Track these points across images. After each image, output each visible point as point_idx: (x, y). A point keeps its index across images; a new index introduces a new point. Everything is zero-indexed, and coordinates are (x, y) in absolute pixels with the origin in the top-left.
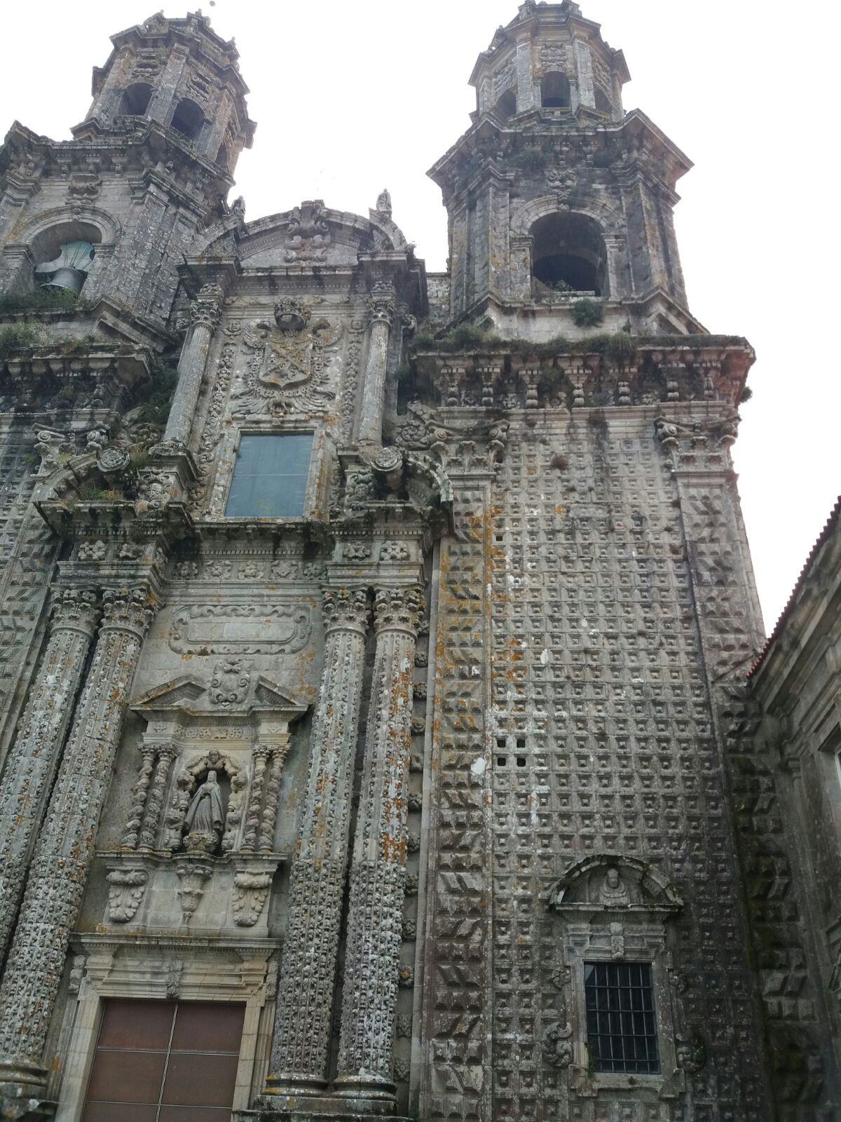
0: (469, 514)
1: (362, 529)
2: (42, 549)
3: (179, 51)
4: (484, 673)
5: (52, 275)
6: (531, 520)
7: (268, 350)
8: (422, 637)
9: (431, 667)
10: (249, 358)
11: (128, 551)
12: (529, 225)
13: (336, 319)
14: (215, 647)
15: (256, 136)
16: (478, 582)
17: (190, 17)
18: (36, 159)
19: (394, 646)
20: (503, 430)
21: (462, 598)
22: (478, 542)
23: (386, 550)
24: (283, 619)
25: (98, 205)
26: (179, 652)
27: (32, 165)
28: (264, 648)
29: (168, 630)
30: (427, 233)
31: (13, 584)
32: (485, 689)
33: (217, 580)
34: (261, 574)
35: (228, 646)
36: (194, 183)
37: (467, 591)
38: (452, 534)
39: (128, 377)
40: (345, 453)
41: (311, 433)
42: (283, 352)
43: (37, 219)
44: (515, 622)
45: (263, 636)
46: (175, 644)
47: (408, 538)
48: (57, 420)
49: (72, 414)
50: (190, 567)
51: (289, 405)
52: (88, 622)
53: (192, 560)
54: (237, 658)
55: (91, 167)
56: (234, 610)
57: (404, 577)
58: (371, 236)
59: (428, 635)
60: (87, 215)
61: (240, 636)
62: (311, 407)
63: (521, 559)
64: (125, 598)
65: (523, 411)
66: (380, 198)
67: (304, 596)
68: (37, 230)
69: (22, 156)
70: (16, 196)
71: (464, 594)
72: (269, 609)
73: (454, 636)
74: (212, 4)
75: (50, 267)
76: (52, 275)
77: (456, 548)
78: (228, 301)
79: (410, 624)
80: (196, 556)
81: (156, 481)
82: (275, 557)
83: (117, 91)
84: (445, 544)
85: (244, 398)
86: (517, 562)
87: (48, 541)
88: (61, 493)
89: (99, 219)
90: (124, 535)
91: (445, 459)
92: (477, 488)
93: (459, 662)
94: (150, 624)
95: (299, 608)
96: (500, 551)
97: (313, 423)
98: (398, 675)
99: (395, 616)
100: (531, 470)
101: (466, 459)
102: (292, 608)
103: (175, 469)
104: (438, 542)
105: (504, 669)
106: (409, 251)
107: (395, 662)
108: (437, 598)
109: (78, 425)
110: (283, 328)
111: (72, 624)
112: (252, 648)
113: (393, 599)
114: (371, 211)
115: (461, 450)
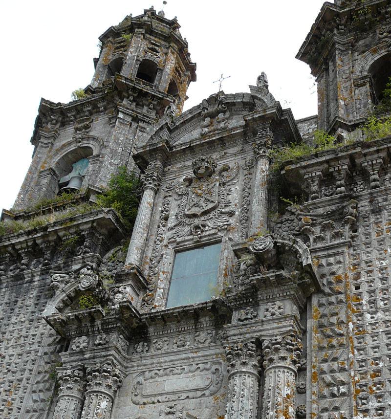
0: (333, 274)
1: (250, 297)
2: (56, 347)
3: (139, 33)
4: (349, 391)
5: (67, 183)
6: (381, 269)
7: (190, 193)
8: (302, 370)
9: (308, 392)
10: (179, 202)
11: (101, 339)
12: (367, 68)
13: (231, 162)
14: (160, 398)
15: (197, 72)
16: (342, 322)
17: (146, 11)
18: (56, 118)
19: (281, 381)
20: (353, 208)
21: (329, 336)
22: (340, 293)
23: (267, 310)
24: (205, 372)
25: (91, 134)
26: (138, 404)
27: (54, 122)
28: (191, 394)
29: (131, 390)
30: (298, 93)
31: (39, 373)
32: (351, 403)
33: (159, 352)
34: (188, 343)
35: (168, 396)
36: (148, 106)
37: (333, 331)
38: (319, 291)
39: (104, 231)
40: (237, 248)
41: (220, 241)
42: (200, 192)
43: (58, 151)
44: (373, 348)
45: (191, 387)
46: (135, 399)
47: (283, 298)
48: (64, 267)
49: (72, 261)
50: (143, 345)
51: (204, 226)
52: (79, 390)
53: (144, 342)
54: (172, 404)
55: (87, 113)
56: (171, 371)
57: (282, 327)
58: (254, 105)
59: (306, 369)
60: (85, 142)
61: (175, 388)
62: (219, 224)
63: (375, 300)
64: (98, 371)
65: (369, 191)
66: (259, 78)
67: (217, 354)
68: (57, 159)
69: (48, 118)
70: (46, 142)
71: (331, 334)
72: (195, 367)
73: (325, 367)
74: (165, 3)
75: (67, 178)
76: (67, 183)
77: (324, 300)
78: (166, 169)
79: (288, 361)
80: (147, 340)
81: (119, 292)
82: (196, 330)
83: (104, 66)
84: (315, 301)
85: (176, 228)
86: (372, 302)
87: (58, 343)
88: (60, 310)
89: (92, 142)
90: (98, 330)
91: (312, 238)
92: (337, 254)
93: (329, 385)
94: (119, 387)
95: (214, 363)
96: (358, 298)
97: (220, 234)
98: (279, 399)
99: (276, 357)
100: (379, 233)
101: (328, 235)
102: (209, 364)
103: (130, 282)
104: (309, 299)
105: (366, 385)
106: (278, 105)
107: (277, 391)
108: (311, 340)
109: (75, 267)
110: (200, 178)
111: (69, 393)
112: (184, 396)
113: (274, 344)
114: (251, 87)
115: (323, 230)
